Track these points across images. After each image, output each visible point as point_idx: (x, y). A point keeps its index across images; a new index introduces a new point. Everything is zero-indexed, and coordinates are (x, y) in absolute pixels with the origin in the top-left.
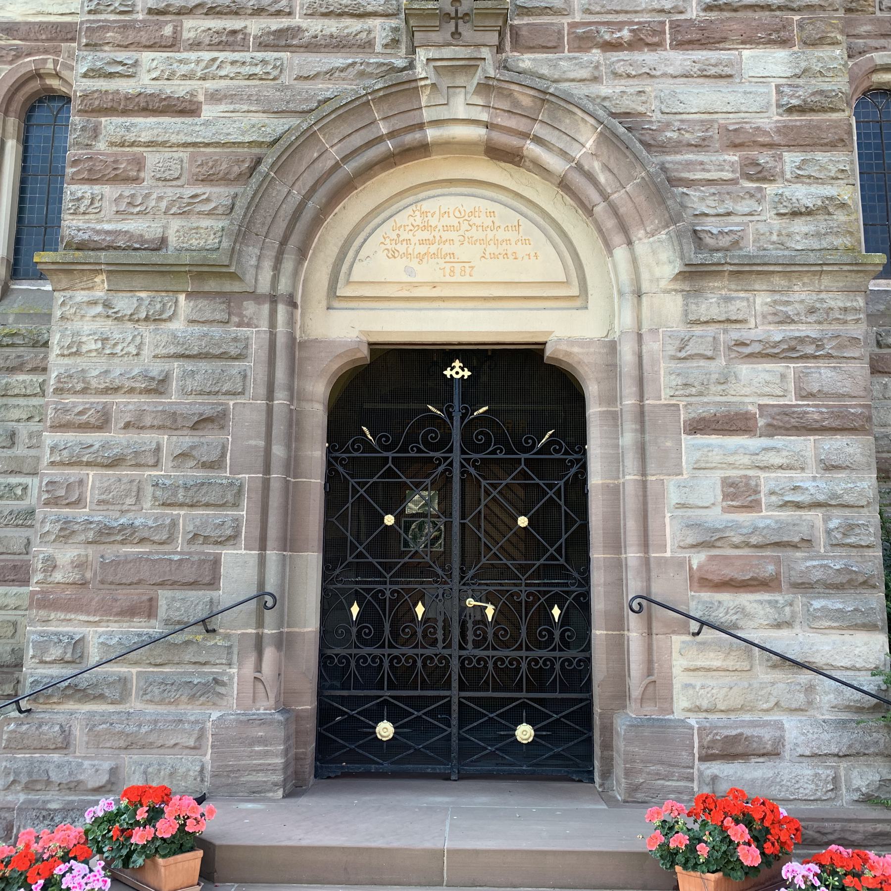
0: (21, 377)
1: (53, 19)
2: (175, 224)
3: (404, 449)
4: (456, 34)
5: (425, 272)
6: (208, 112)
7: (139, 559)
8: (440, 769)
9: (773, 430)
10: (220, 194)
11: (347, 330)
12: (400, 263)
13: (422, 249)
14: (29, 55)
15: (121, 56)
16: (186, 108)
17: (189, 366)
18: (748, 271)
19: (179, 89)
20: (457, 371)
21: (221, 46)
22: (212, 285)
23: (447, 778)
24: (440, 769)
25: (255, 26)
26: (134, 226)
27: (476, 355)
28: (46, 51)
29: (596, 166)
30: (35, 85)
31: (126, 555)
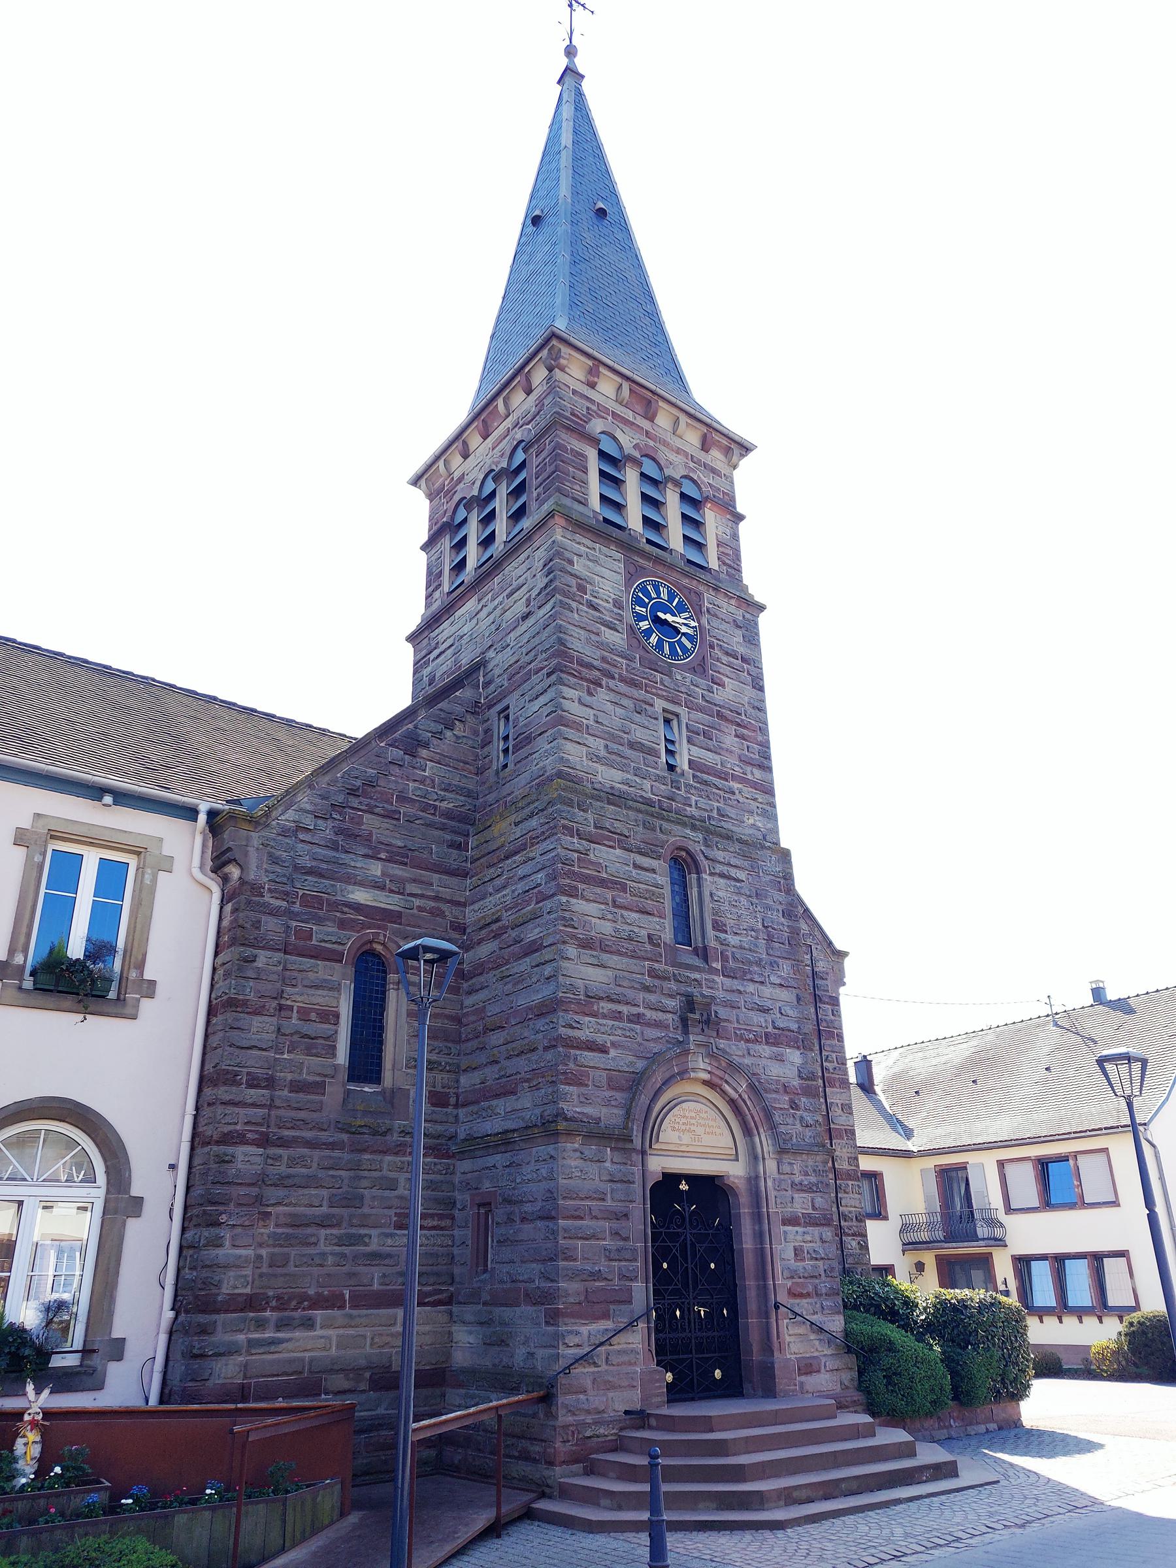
0: (367, 1156)
1: (383, 906)
2: (604, 1110)
3: (668, 1228)
4: (703, 1030)
5: (686, 1139)
6: (613, 1053)
7: (603, 1289)
8: (691, 1395)
9: (807, 1224)
10: (619, 1095)
11: (657, 1165)
12: (677, 1133)
13: (683, 1127)
14: (369, 928)
15: (577, 1018)
16: (603, 1050)
17: (614, 1186)
18: (797, 1152)
19: (600, 1039)
20: (684, 1187)
21: (614, 1018)
22: (620, 1145)
23: (693, 1399)
24: (691, 1395)
25: (625, 1009)
26: (588, 1110)
27: (691, 1179)
28: (379, 928)
29: (746, 1097)
30: (367, 947)
31: (597, 1287)
